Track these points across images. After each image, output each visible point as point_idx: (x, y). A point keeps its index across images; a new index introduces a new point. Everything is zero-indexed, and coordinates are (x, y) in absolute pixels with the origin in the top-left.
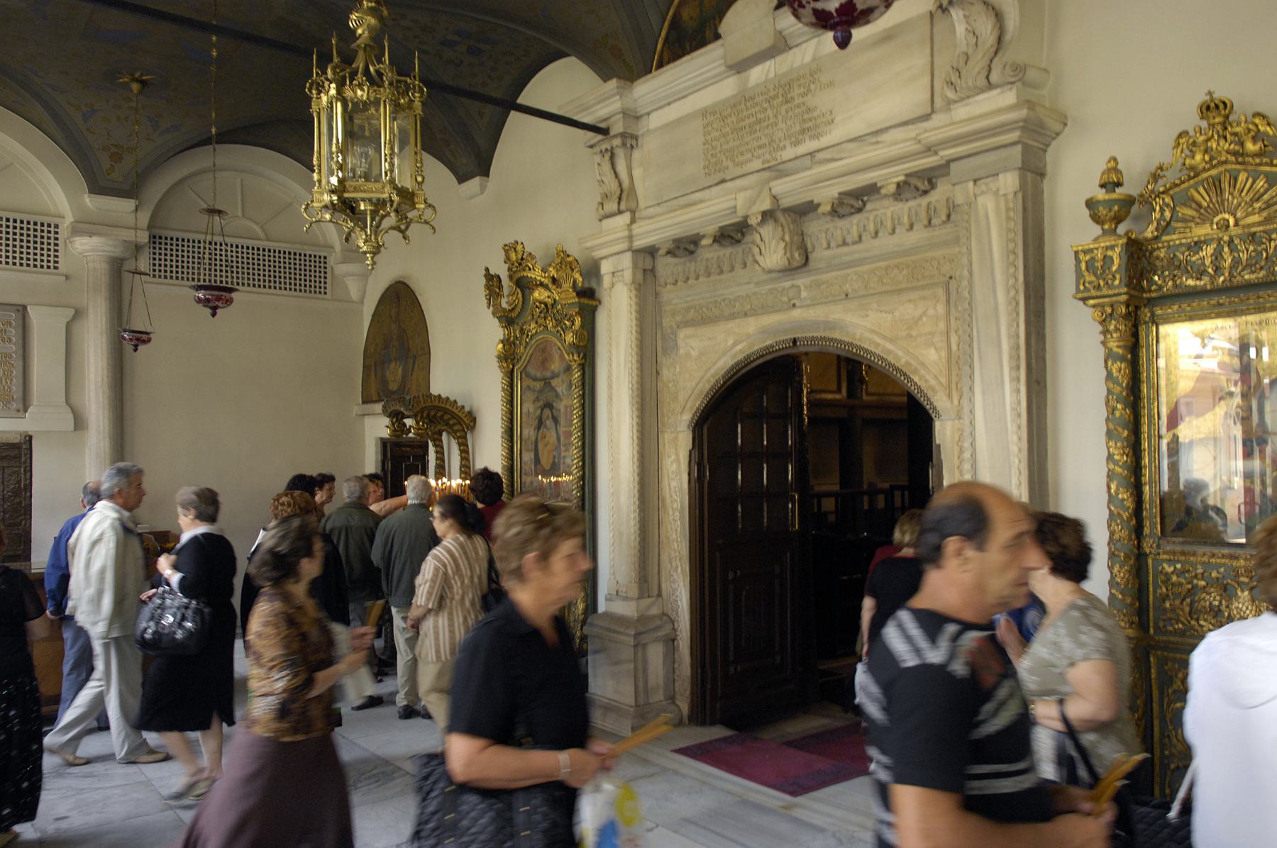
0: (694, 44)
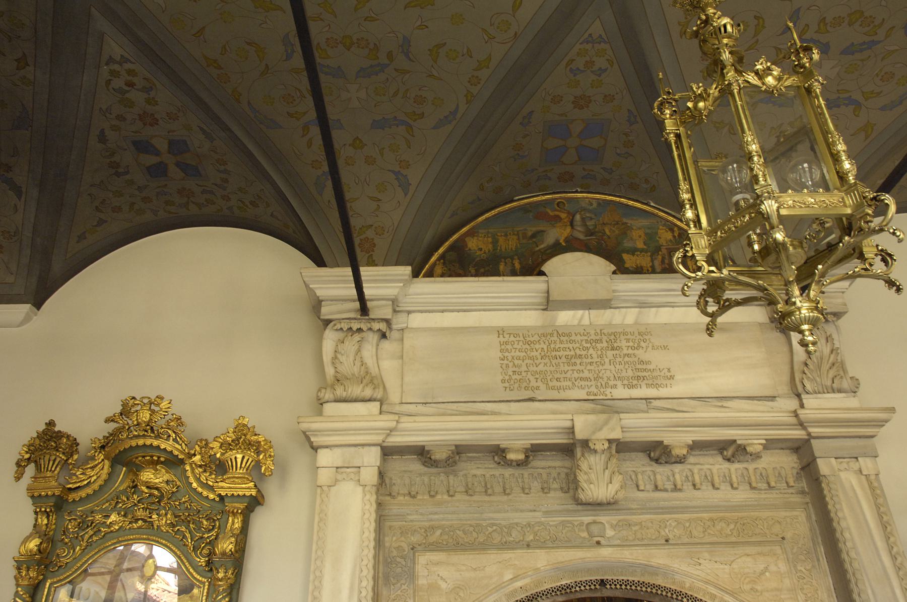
0: (482, 270)
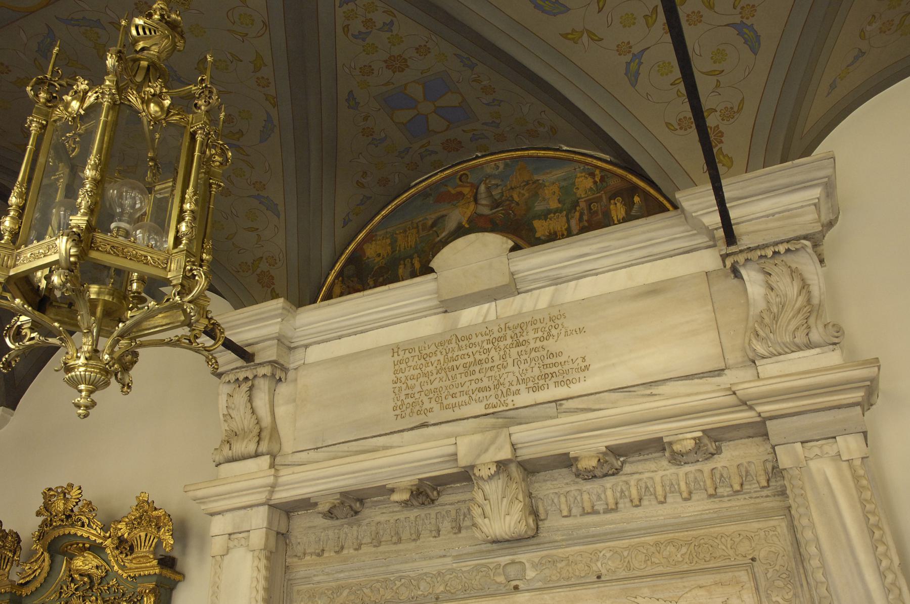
0: (381, 279)
